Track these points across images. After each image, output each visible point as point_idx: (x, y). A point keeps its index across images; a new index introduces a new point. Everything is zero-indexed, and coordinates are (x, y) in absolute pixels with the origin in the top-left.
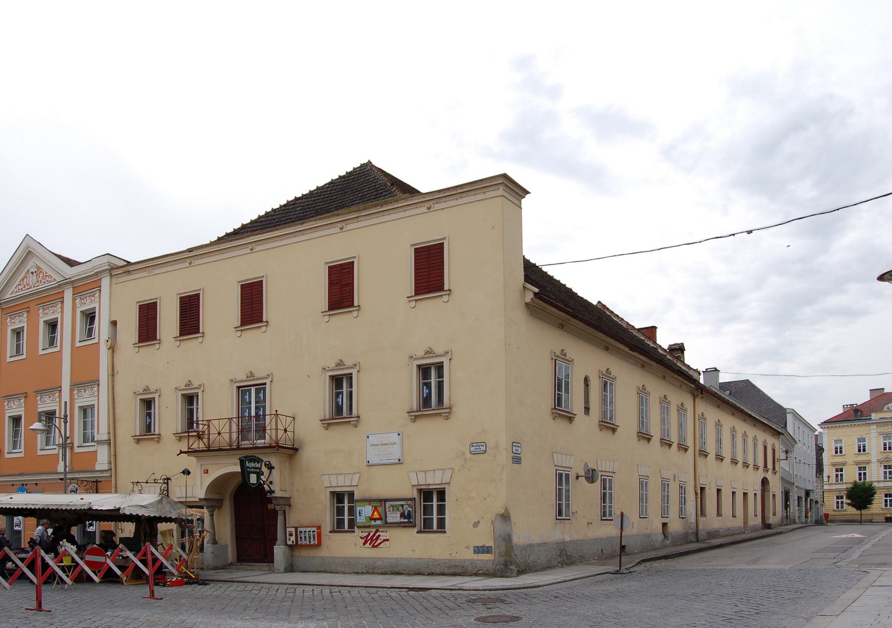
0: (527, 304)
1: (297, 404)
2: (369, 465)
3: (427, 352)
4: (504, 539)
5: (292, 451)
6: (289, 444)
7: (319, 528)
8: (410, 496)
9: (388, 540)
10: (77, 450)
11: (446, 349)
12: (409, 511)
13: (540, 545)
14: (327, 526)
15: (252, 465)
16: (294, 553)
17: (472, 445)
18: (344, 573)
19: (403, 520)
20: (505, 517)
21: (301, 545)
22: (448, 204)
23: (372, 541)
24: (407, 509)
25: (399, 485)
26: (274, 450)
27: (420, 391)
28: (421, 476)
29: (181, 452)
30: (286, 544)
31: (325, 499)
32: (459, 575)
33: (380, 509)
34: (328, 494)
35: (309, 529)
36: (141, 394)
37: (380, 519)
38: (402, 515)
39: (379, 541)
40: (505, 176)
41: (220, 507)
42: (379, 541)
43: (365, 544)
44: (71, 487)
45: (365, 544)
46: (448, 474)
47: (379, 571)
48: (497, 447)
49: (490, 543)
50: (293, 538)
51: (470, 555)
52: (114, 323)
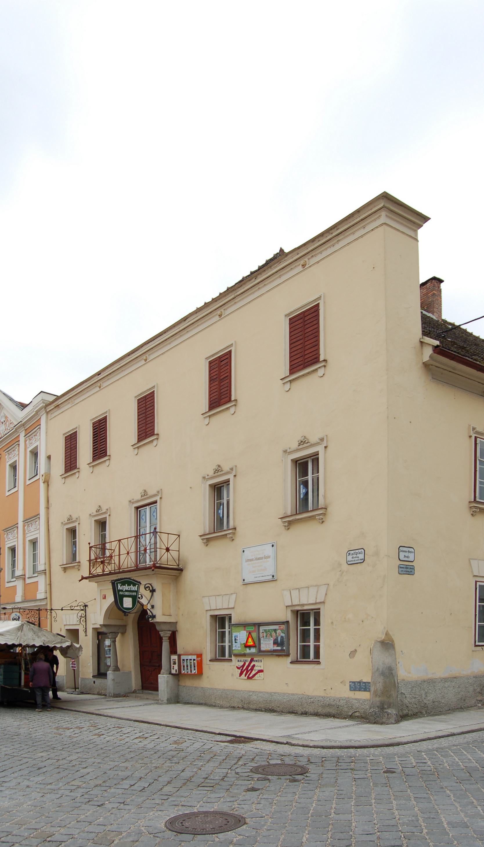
0: (426, 365)
1: (184, 517)
2: (246, 585)
3: (301, 443)
4: (383, 674)
5: (176, 572)
6: (172, 564)
7: (200, 656)
8: (284, 620)
9: (261, 671)
10: (28, 581)
11: (321, 436)
12: (282, 637)
13: (445, 680)
14: (207, 656)
15: (126, 587)
16: (181, 683)
17: (349, 553)
18: (221, 707)
19: (276, 648)
20: (387, 644)
21: (184, 674)
22: (325, 254)
23: (247, 671)
24: (280, 634)
25: (272, 606)
26: (149, 572)
27: (297, 491)
28: (295, 593)
29: (83, 578)
30: (170, 673)
31: (206, 623)
32: (334, 716)
33: (254, 635)
34: (208, 618)
35: (190, 657)
36: (67, 524)
37: (254, 646)
38: (275, 643)
39: (254, 672)
40: (385, 196)
41: (123, 633)
42: (254, 672)
43: (241, 674)
44: (13, 615)
45: (241, 674)
46: (323, 590)
47: (254, 707)
48: (377, 554)
49: (367, 679)
50: (176, 667)
51: (343, 693)
52: (49, 457)
